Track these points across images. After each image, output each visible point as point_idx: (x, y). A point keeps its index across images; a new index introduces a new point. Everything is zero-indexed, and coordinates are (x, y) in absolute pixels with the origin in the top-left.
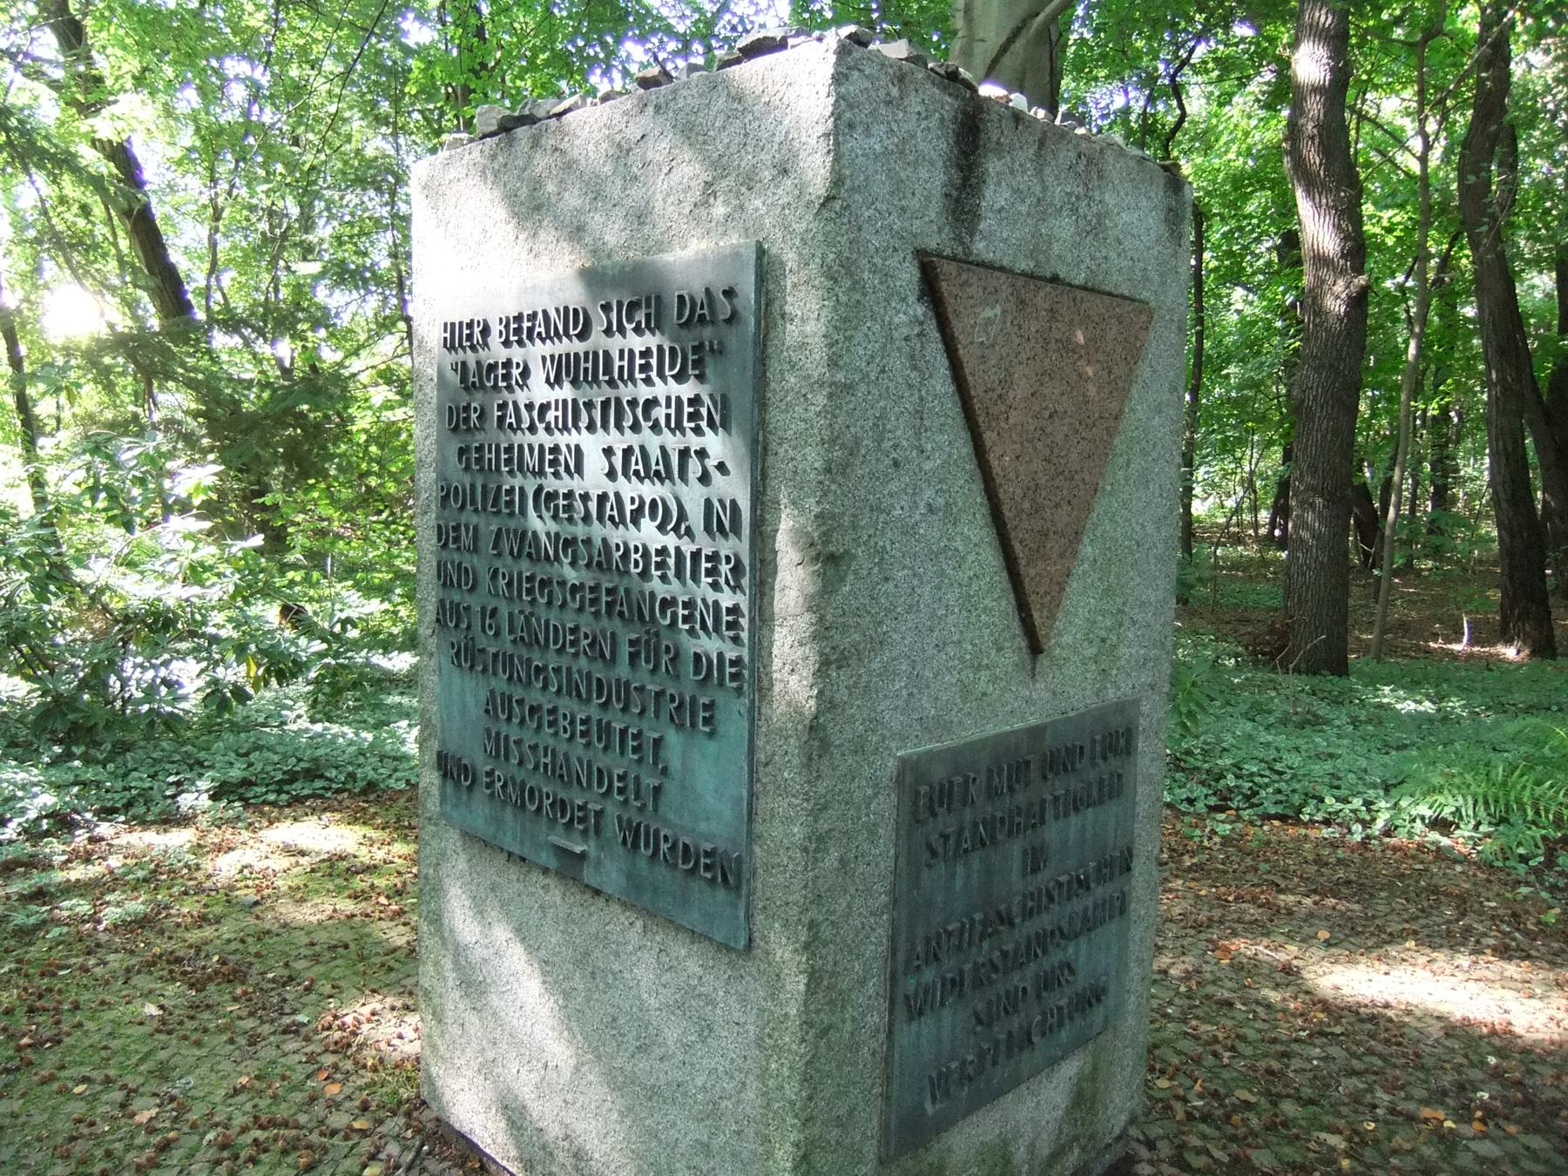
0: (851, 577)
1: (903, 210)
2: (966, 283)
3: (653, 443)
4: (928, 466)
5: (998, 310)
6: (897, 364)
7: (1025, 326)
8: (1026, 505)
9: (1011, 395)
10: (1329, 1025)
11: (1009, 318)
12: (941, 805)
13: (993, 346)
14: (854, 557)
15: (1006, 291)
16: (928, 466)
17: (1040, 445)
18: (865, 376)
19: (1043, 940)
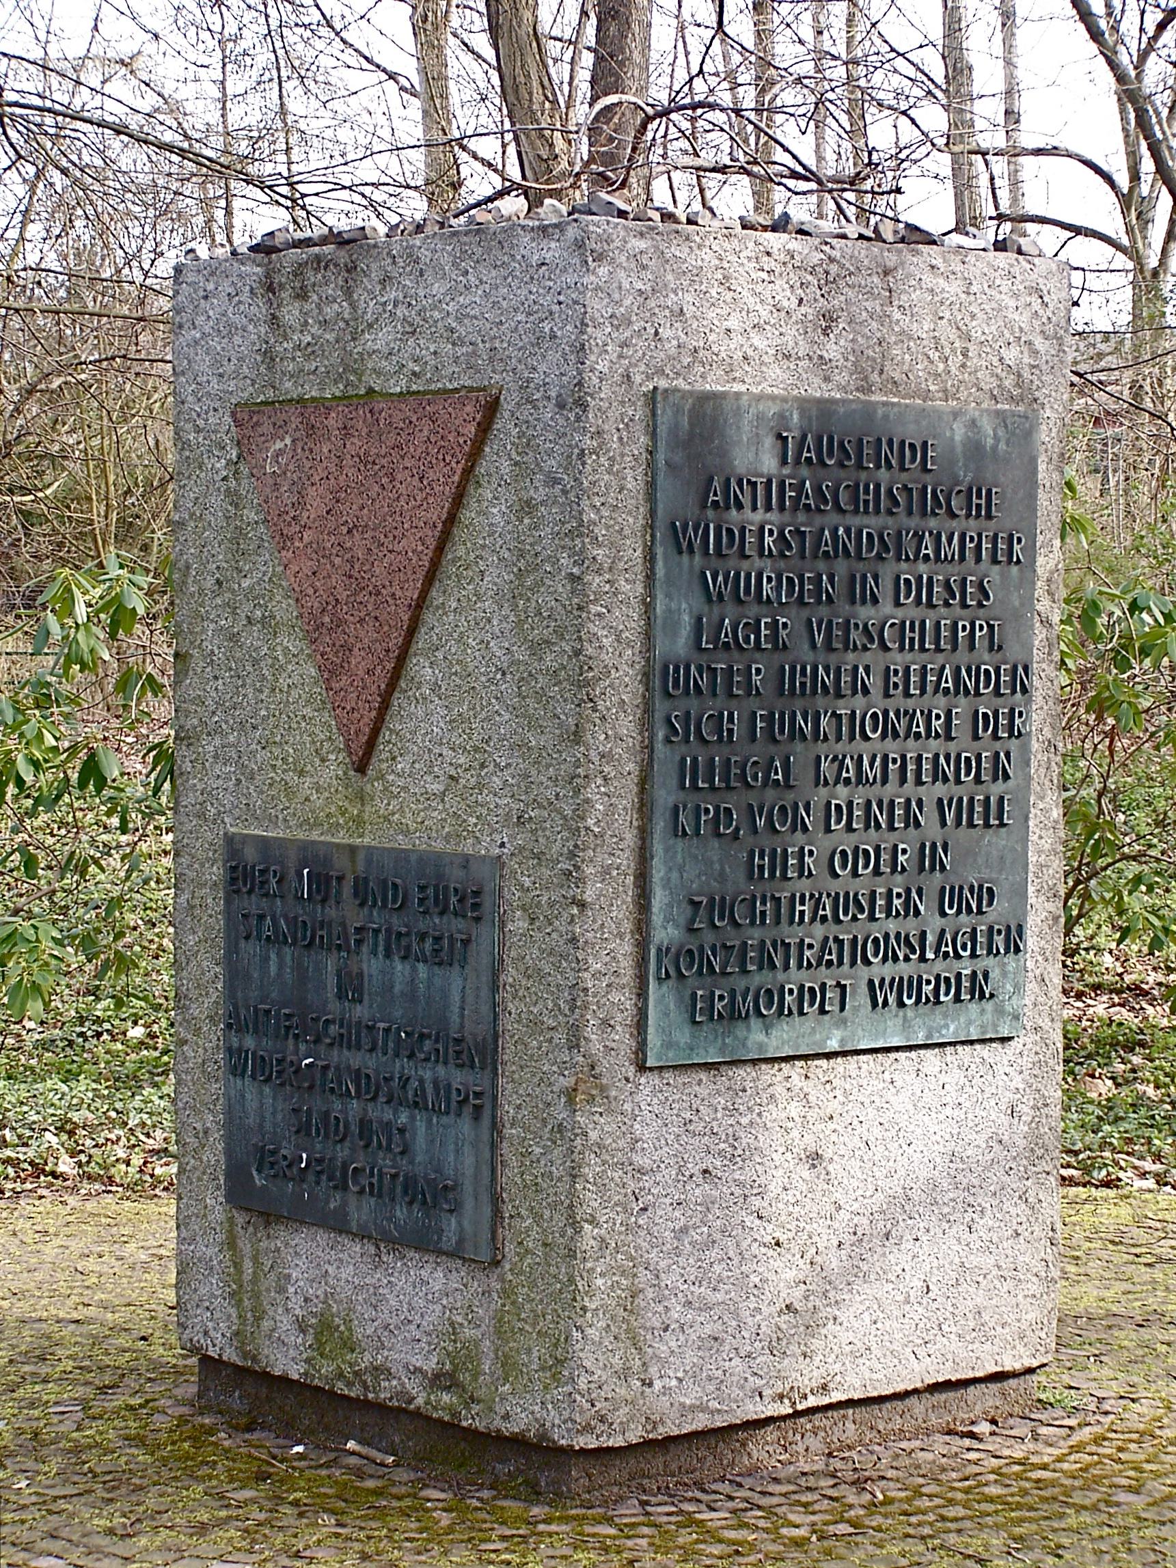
0: (191, 673)
1: (221, 375)
2: (257, 424)
3: (910, 612)
4: (246, 583)
5: (288, 441)
6: (216, 501)
7: (316, 449)
8: (327, 619)
9: (305, 514)
10: (697, 1542)
11: (300, 444)
12: (909, 997)
13: (285, 473)
14: (192, 656)
15: (295, 421)
16: (246, 583)
17: (337, 561)
18: (192, 515)
19: (370, 1089)
